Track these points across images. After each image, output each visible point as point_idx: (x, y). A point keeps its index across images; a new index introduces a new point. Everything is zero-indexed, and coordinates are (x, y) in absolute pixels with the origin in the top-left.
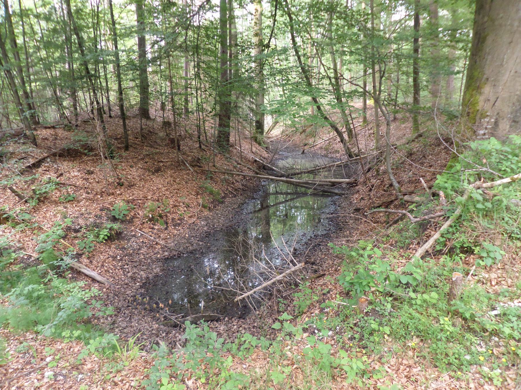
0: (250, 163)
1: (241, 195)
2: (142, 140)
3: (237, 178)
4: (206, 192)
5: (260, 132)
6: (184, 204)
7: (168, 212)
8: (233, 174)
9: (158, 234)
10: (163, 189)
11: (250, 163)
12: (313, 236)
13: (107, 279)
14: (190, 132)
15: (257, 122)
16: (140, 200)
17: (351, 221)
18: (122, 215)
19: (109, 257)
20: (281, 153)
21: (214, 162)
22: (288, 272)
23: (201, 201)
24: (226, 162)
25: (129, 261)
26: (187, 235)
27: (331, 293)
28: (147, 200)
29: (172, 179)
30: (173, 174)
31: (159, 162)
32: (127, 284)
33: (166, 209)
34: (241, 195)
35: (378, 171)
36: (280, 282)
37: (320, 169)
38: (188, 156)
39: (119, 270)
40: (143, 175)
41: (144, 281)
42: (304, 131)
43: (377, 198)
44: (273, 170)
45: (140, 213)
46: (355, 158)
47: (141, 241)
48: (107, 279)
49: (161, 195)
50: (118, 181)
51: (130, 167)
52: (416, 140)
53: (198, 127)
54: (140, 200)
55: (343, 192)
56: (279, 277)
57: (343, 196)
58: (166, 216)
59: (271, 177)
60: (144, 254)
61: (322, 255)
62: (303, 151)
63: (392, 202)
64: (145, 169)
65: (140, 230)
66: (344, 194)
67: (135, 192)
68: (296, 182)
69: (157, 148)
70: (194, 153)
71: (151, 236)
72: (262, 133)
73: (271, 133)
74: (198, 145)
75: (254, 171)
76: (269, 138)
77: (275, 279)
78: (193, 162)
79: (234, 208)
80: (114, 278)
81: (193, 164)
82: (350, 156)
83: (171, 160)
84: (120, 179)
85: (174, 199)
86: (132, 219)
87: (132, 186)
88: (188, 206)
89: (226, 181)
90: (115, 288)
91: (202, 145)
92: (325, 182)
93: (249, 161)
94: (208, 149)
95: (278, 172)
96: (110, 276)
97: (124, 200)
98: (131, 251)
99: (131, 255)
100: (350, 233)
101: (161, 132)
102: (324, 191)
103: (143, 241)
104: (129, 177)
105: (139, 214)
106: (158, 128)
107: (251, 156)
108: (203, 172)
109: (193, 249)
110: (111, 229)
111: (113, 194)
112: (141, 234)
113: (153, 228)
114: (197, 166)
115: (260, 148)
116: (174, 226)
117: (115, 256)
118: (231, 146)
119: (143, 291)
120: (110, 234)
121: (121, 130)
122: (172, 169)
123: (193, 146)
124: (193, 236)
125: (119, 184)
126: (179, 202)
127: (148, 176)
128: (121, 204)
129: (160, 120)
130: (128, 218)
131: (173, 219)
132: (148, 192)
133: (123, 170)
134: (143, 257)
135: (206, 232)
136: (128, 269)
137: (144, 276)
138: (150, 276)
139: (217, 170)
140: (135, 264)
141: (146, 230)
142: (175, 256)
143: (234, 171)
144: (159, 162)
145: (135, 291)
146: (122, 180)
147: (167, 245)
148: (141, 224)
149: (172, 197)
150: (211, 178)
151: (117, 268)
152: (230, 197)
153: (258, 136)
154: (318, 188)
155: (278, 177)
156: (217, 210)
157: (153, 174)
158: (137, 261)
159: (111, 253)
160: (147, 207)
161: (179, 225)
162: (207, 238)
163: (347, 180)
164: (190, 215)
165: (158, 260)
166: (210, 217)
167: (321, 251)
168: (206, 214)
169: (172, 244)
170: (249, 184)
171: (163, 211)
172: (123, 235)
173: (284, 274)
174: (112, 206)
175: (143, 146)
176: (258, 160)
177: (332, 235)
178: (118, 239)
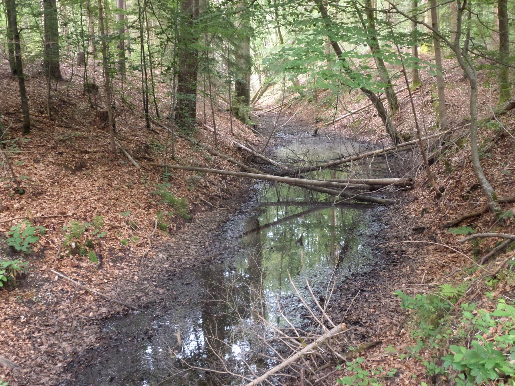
0: (230, 153)
1: (221, 206)
2: (51, 115)
3: (212, 177)
4: (163, 203)
5: (244, 101)
6: (127, 224)
7: (102, 238)
8: (206, 172)
9: (87, 277)
10: (93, 199)
11: (230, 153)
12: (349, 275)
13: (6, 357)
14: (129, 101)
15: (238, 83)
16: (55, 217)
17: (411, 250)
18: (26, 244)
19: (6, 319)
20: (277, 135)
21: (173, 152)
22: (321, 339)
23: (155, 218)
24: (192, 152)
25: (40, 325)
26: (136, 277)
27: (401, 376)
28: (66, 217)
29: (106, 181)
30: (106, 173)
31: (82, 152)
32: (40, 365)
33: (99, 233)
34: (221, 206)
35: (448, 164)
36: (307, 357)
37: (349, 161)
38: (130, 142)
39: (24, 340)
40: (57, 175)
41: (68, 360)
42: (316, 98)
43: (451, 209)
44: (270, 164)
45: (56, 240)
46: (404, 143)
47: (60, 288)
48: (6, 357)
49: (89, 208)
50: (15, 186)
51: (35, 161)
52: (508, 112)
53: (145, 93)
54: (55, 217)
55: (391, 200)
56: (307, 349)
57: (391, 207)
58: (100, 245)
59: (269, 176)
60: (65, 312)
61: (369, 307)
62: (316, 131)
63: (479, 216)
64: (59, 165)
65: (56, 269)
66: (392, 204)
67: (45, 205)
68: (311, 184)
69: (77, 129)
70: (139, 136)
71: (76, 280)
72: (246, 102)
73: (260, 101)
74: (144, 124)
75: (239, 166)
76: (256, 110)
77: (299, 353)
78: (138, 152)
79: (211, 230)
80: (17, 355)
81: (139, 156)
82: (396, 140)
83: (102, 148)
84: (19, 183)
85: (111, 215)
86: (43, 251)
87: (40, 194)
88: (134, 228)
89: (194, 182)
90: (20, 372)
91: (151, 124)
92: (357, 182)
93: (229, 149)
94: (160, 130)
95: (276, 166)
96: (11, 352)
97: (27, 218)
98: (44, 307)
99: (43, 313)
100: (412, 270)
101: (82, 102)
102: (358, 199)
103: (62, 290)
104: (33, 179)
105: (53, 242)
106: (76, 95)
107: (231, 141)
108: (156, 169)
109: (149, 300)
110: (8, 269)
111: (8, 209)
112: (59, 277)
113: (78, 267)
114: (145, 158)
115: (243, 127)
116: (113, 261)
117: (16, 316)
118: (200, 124)
119: (69, 378)
120: (7, 277)
121: (15, 99)
122: (104, 165)
123: (136, 124)
124: (146, 279)
125: (17, 191)
126: (120, 221)
127: (65, 176)
128: (23, 226)
129: (79, 81)
130: (36, 250)
131: (111, 250)
132: (66, 204)
133: (22, 167)
134: (63, 317)
135: (167, 272)
136: (40, 337)
137: (69, 349)
138: (79, 349)
139: (178, 166)
140: (52, 330)
141: (67, 270)
142: (118, 313)
143: (205, 166)
144: (82, 152)
145: (56, 377)
146: (23, 185)
147: (104, 295)
148: (58, 260)
149: (107, 212)
150: (170, 179)
151: (20, 337)
152: (202, 211)
153: (241, 106)
154: (349, 193)
155: (277, 175)
156: (183, 233)
157: (74, 173)
158: (54, 324)
159: (9, 312)
160: (66, 231)
161: (122, 259)
162: (171, 282)
163: (397, 180)
164: (138, 243)
165: (91, 321)
166: (172, 245)
167: (367, 301)
168: (165, 239)
169: (113, 293)
170: (232, 188)
171: (93, 236)
172: (29, 280)
173: (314, 344)
174: (8, 230)
175: (53, 125)
176: (243, 147)
177: (381, 274)
178: (20, 286)
